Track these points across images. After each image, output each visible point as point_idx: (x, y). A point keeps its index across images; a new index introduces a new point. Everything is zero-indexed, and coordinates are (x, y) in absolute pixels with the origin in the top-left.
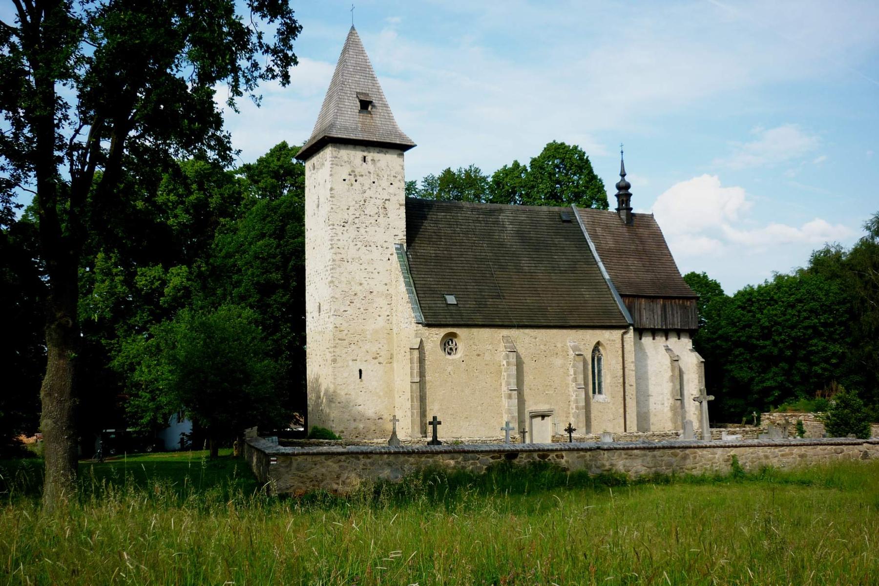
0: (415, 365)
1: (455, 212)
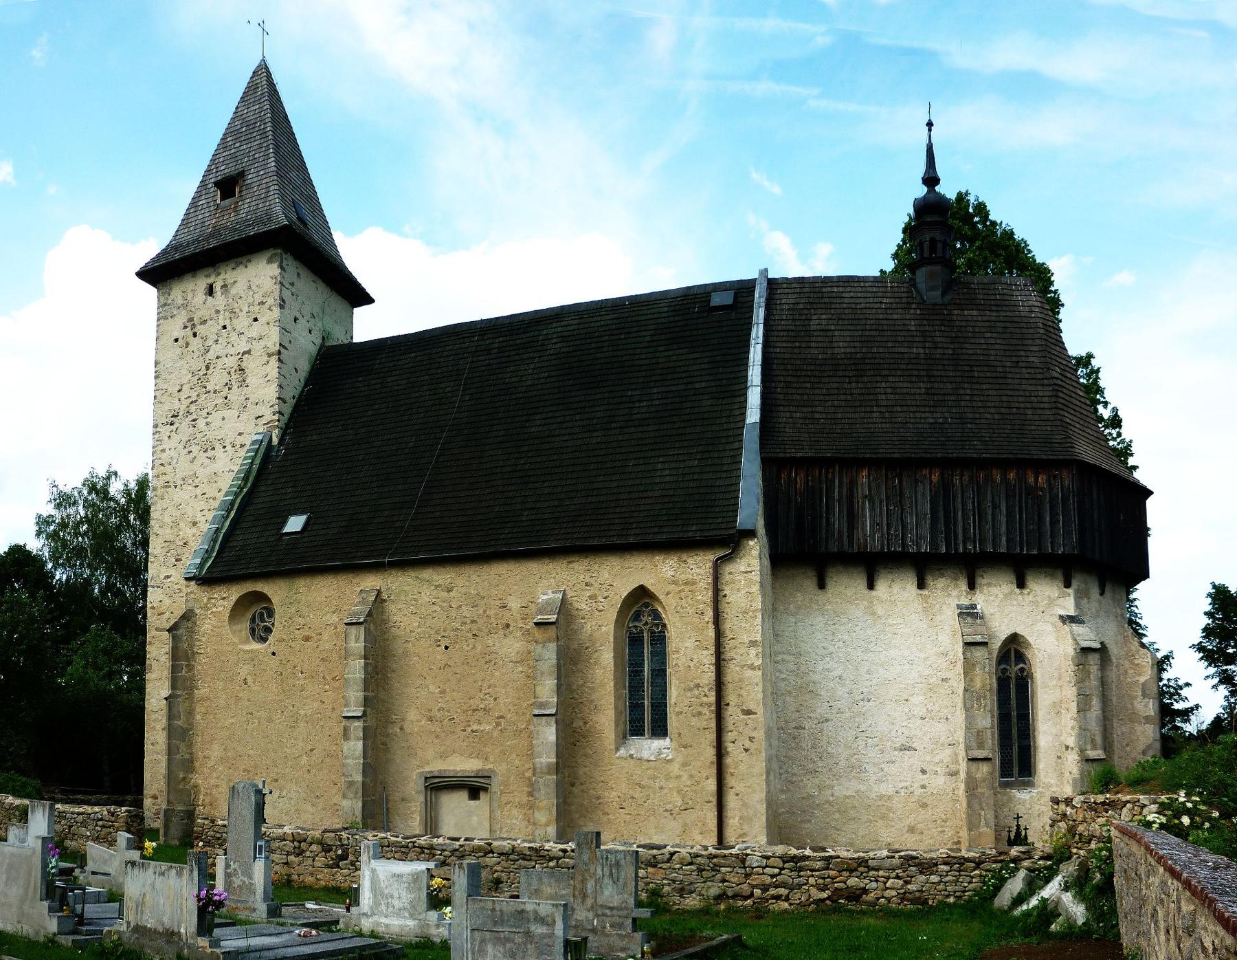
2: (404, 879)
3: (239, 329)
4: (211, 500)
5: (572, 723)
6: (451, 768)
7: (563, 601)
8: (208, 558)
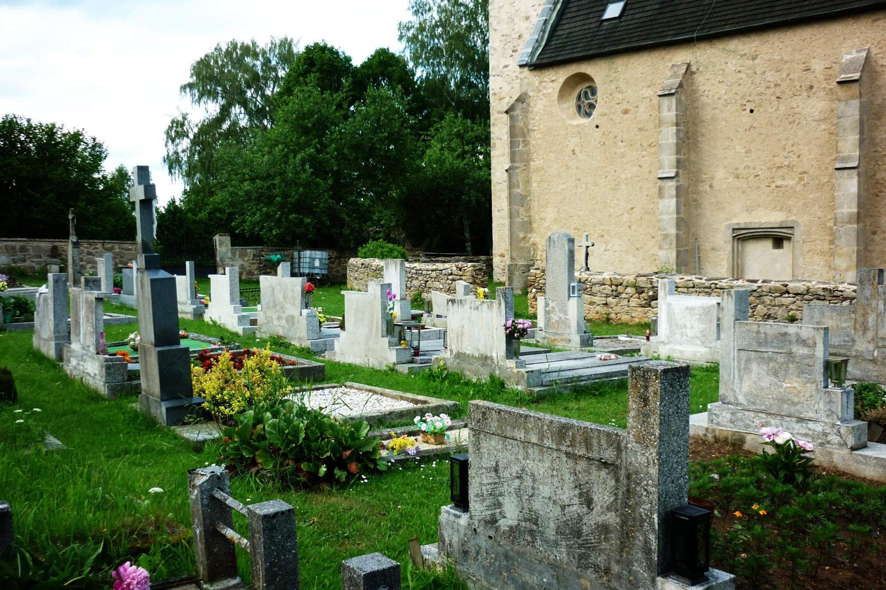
2: (696, 312)
5: (875, 175)
6: (756, 221)
7: (867, 59)
8: (539, 46)
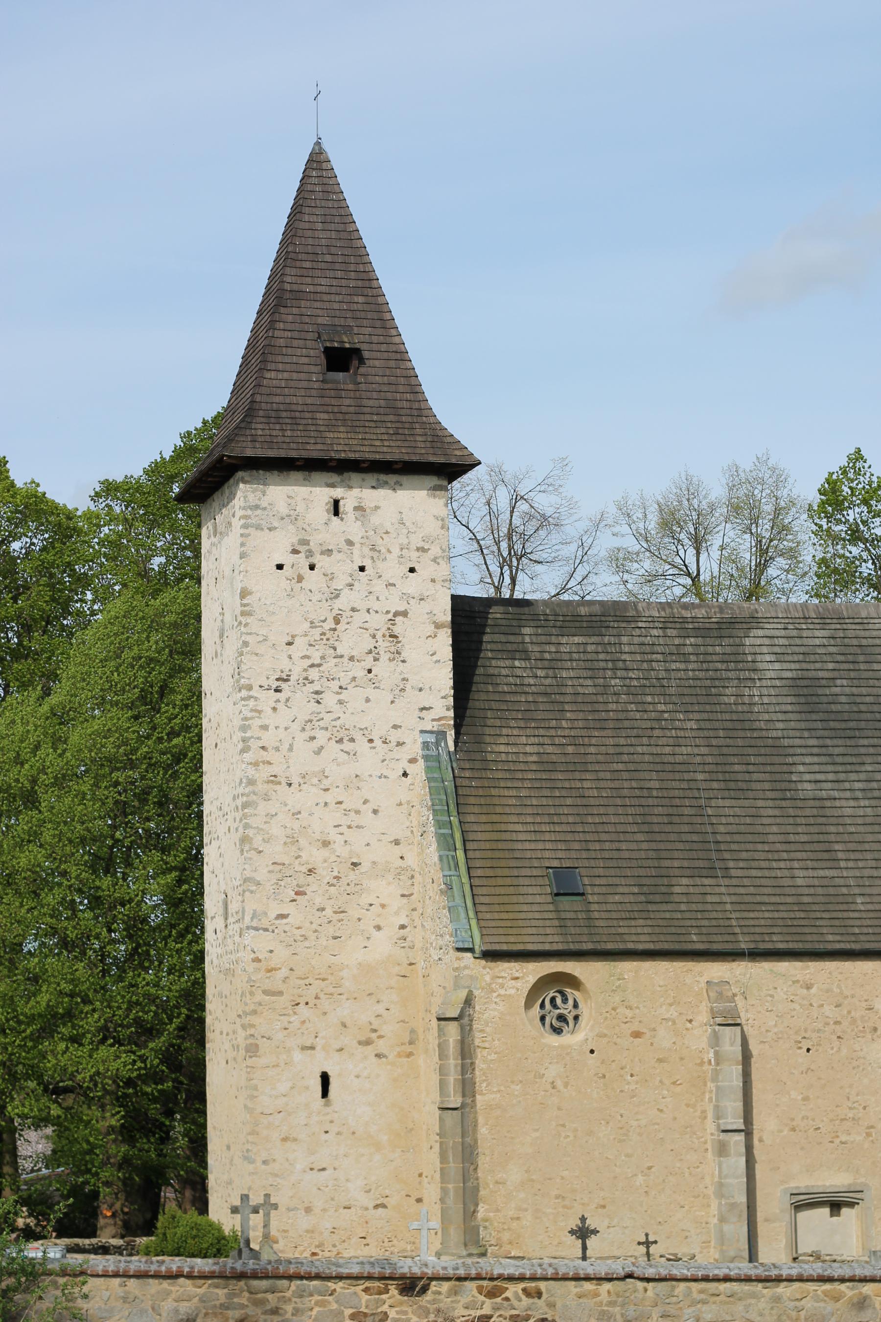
0: (452, 1062)
1: (615, 632)
3: (388, 576)
4: (352, 814)
6: (820, 1183)
